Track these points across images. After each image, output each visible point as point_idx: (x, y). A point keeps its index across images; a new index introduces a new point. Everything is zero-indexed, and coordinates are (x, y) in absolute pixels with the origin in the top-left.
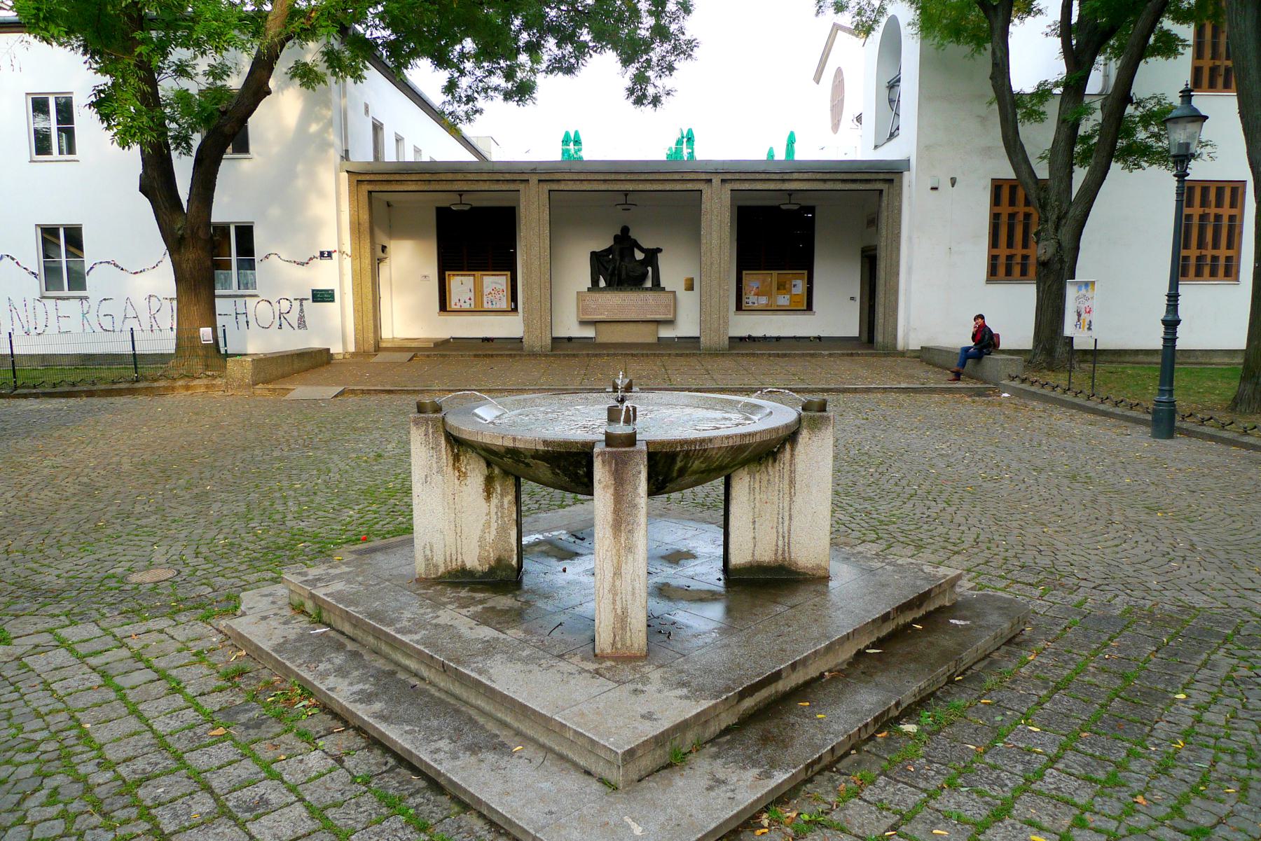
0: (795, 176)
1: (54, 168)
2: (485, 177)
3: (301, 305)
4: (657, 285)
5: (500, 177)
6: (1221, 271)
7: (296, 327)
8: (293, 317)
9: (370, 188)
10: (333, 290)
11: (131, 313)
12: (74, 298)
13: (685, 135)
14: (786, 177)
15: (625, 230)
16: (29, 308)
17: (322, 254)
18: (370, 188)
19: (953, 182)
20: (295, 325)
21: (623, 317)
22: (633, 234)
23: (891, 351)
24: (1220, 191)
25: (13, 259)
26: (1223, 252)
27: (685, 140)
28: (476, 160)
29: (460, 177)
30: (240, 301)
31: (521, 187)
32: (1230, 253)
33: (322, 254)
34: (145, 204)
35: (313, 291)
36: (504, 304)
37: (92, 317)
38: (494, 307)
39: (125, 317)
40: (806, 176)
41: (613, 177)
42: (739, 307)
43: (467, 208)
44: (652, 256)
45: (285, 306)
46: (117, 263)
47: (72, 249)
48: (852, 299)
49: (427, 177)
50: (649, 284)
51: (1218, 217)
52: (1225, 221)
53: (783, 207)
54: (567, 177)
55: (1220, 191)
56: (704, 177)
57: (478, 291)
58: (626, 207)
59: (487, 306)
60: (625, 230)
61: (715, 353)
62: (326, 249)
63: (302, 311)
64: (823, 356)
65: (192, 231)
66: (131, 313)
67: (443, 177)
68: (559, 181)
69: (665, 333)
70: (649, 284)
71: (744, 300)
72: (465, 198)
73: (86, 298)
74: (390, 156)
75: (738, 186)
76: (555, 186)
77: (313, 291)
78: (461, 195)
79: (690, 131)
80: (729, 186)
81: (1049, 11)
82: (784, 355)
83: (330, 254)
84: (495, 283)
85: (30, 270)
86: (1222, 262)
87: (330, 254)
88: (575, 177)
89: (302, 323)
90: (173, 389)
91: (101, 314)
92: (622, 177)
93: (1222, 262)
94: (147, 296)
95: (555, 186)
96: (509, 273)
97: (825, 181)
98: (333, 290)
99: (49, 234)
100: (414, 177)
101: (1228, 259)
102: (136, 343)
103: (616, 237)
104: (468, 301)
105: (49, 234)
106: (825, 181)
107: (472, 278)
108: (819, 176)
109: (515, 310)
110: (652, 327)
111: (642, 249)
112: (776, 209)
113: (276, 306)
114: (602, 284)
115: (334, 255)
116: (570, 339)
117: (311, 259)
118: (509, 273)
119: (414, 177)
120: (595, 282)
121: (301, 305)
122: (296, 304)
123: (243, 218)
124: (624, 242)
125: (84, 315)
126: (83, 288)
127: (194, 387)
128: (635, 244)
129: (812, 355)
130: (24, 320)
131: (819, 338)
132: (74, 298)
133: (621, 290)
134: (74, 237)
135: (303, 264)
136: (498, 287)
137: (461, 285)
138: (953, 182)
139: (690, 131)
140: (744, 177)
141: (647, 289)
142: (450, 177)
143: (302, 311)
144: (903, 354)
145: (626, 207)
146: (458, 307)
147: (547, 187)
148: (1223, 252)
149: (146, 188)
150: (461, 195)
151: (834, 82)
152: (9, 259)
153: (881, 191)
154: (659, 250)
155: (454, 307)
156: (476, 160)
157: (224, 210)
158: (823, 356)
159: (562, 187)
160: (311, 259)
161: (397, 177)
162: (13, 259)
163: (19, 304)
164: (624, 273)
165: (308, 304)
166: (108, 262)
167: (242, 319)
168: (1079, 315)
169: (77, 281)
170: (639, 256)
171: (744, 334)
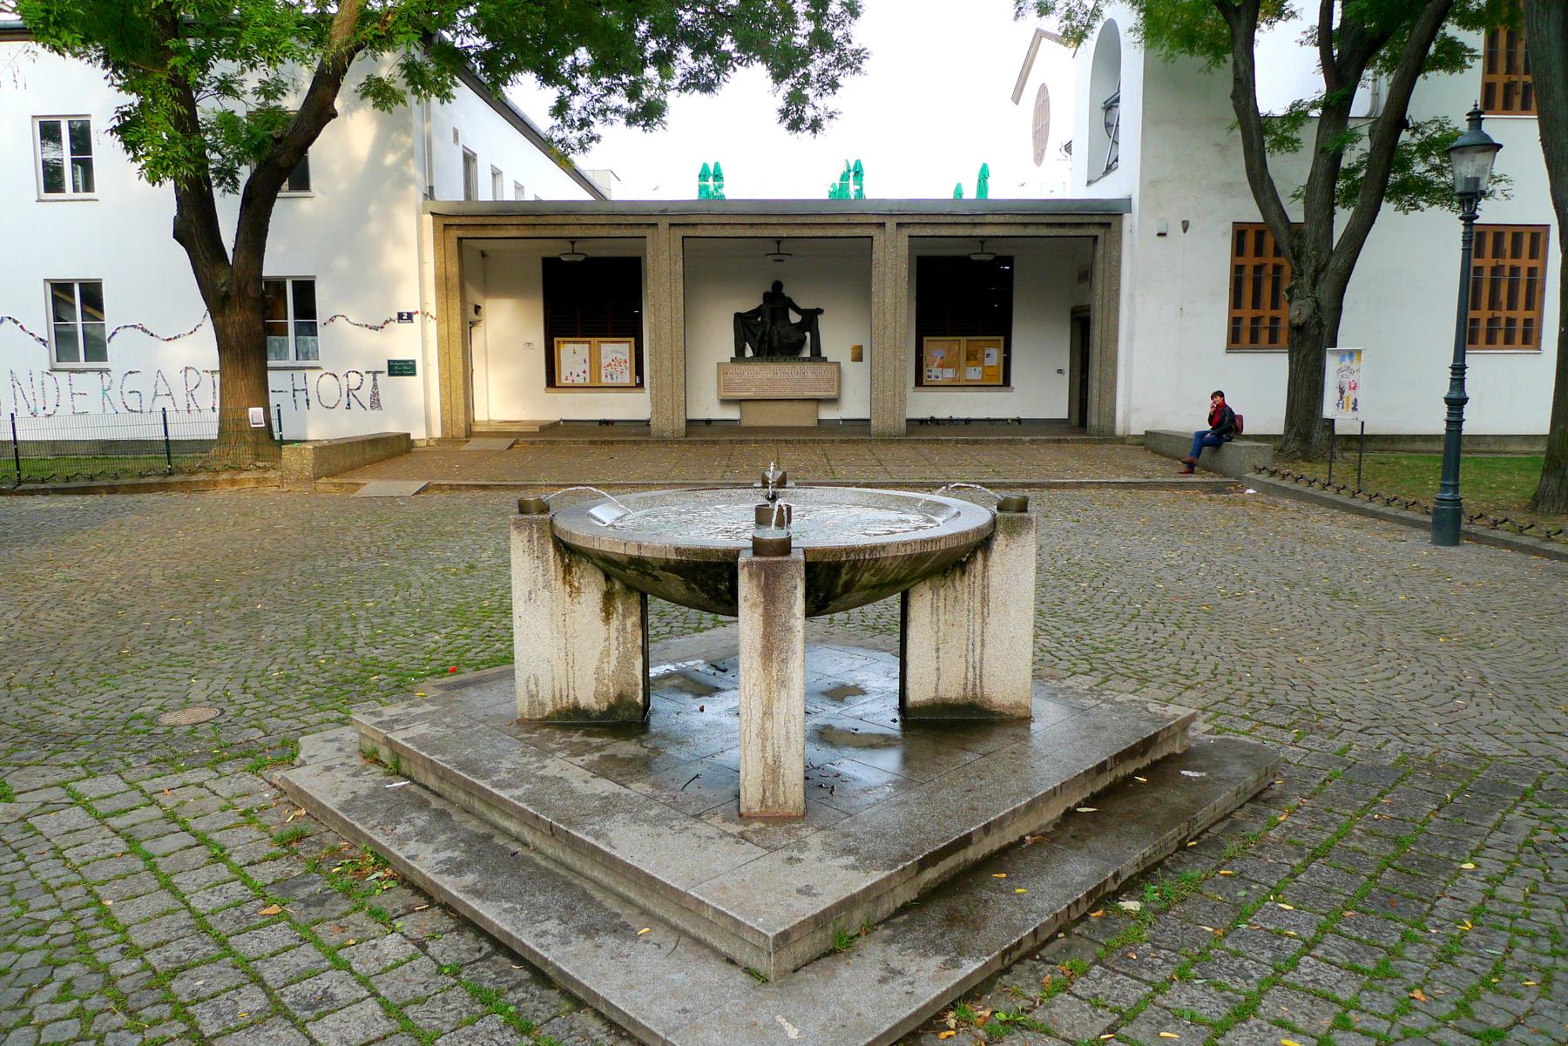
0: (989, 219)
1: (67, 209)
2: (603, 220)
3: (375, 379)
4: (816, 355)
5: (622, 220)
6: (1518, 337)
7: (368, 407)
8: (365, 395)
9: (460, 233)
10: (414, 361)
11: (163, 390)
12: (92, 370)
13: (852, 168)
14: (977, 220)
15: (777, 286)
16: (37, 383)
17: (400, 316)
18: (460, 233)
19: (1186, 226)
20: (367, 404)
21: (775, 395)
22: (788, 291)
23: (1108, 437)
24: (1517, 238)
25: (16, 322)
26: (1520, 314)
27: (852, 174)
28: (592, 198)
29: (571, 220)
30: (298, 375)
31: (648, 232)
32: (1529, 314)
33: (400, 316)
34: (181, 254)
35: (389, 361)
36: (627, 378)
37: (114, 394)
38: (615, 382)
39: (156, 395)
40: (1002, 219)
41: (762, 220)
42: (919, 382)
43: (581, 258)
44: (811, 318)
45: (354, 380)
46: (146, 327)
47: (90, 310)
48: (1060, 371)
49: (531, 220)
50: (806, 353)
51: (1515, 271)
52: (1523, 275)
53: (974, 257)
54: (705, 220)
55: (1517, 238)
56: (875, 220)
57: (594, 361)
58: (779, 257)
59: (605, 381)
60: (777, 286)
61: (889, 439)
62: (405, 309)
63: (375, 386)
64: (1024, 443)
65: (239, 287)
66: (163, 390)
67: (551, 220)
68: (695, 225)
69: (827, 414)
70: (806, 353)
71: (926, 373)
72: (579, 246)
73: (107, 371)
74: (485, 193)
75: (917, 231)
76: (690, 232)
77: (389, 361)
78: (573, 243)
79: (858, 163)
80: (906, 232)
81: (1304, 14)
82: (975, 442)
83: (410, 316)
84: (616, 352)
85: (37, 335)
86: (1520, 325)
87: (410, 316)
88: (716, 220)
89: (375, 402)
90: (215, 484)
91: (126, 391)
92: (774, 220)
93: (1520, 325)
94: (183, 368)
95: (690, 232)
96: (633, 340)
97: (1025, 225)
98: (414, 361)
99: (61, 291)
100: (515, 221)
101: (1528, 322)
102: (169, 426)
103: (766, 295)
104: (582, 375)
105: (61, 291)
106: (1025, 225)
107: (587, 346)
108: (1018, 219)
109: (640, 385)
110: (811, 407)
111: (798, 310)
112: (965, 260)
113: (343, 380)
114: (749, 353)
115: (415, 317)
116: (708, 422)
117: (387, 322)
118: (633, 340)
119: (515, 221)
120: (740, 351)
121: (375, 379)
122: (368, 378)
123: (302, 271)
124: (776, 300)
125: (104, 391)
126: (104, 358)
127: (241, 481)
128: (790, 304)
129: (1010, 442)
130: (30, 398)
131: (1019, 421)
132: (92, 370)
133: (772, 361)
134: (92, 295)
135: (376, 329)
136: (620, 357)
137: (573, 355)
138: (1186, 226)
139: (858, 163)
140: (925, 220)
141: (804, 359)
142: (560, 220)
143: (375, 386)
144: (1122, 440)
145: (779, 257)
146: (569, 382)
147: (680, 232)
148: (1520, 314)
149: (181, 234)
150: (573, 243)
151: (1037, 102)
152: (11, 322)
153: (1096, 238)
154: (820, 311)
155: (564, 382)
156: (592, 198)
157: (278, 261)
158: (1024, 443)
159: (699, 232)
160: (387, 322)
161: (494, 221)
162: (16, 322)
163: (23, 378)
164: (775, 339)
165: (384, 379)
166: (135, 326)
167: (301, 396)
168: (1342, 392)
169: (96, 349)
170: (795, 318)
171: (925, 415)
